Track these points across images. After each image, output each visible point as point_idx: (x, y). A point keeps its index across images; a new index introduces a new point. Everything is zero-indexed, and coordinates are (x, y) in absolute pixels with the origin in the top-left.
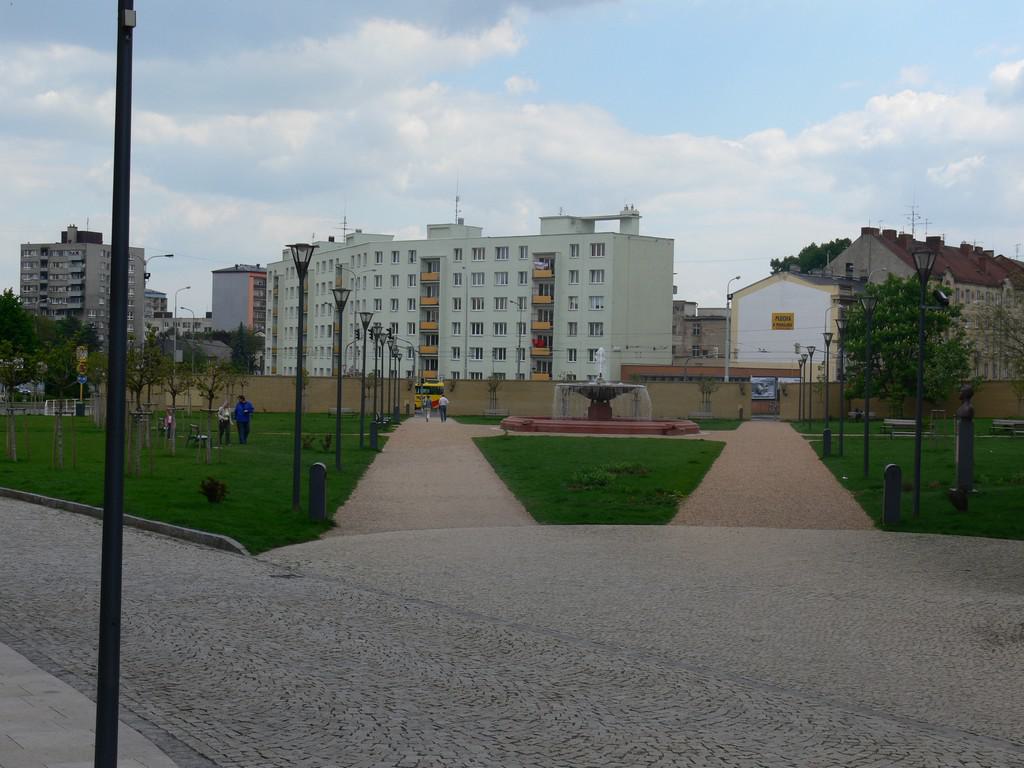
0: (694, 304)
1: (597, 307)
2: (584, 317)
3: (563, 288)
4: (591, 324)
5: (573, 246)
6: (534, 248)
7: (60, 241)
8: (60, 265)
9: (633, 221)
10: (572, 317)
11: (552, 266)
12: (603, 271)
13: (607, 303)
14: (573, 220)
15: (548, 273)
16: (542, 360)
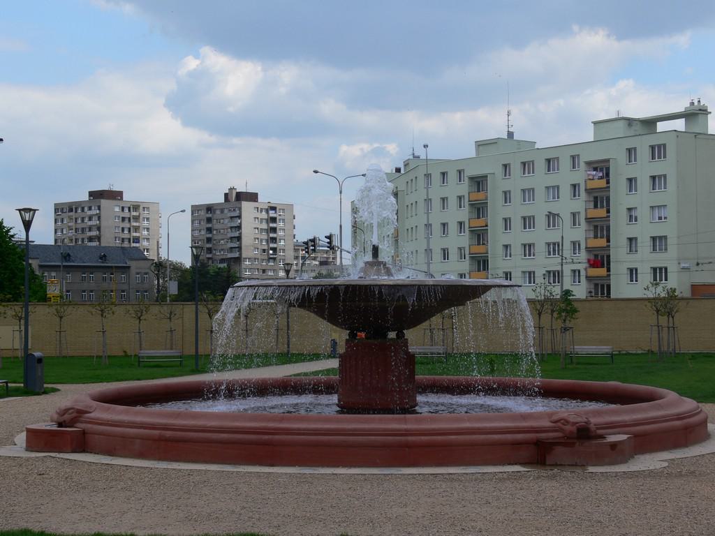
1: (660, 218)
2: (644, 230)
3: (621, 199)
4: (654, 239)
5: (629, 150)
6: (586, 156)
7: (223, 201)
8: (222, 221)
10: (632, 231)
11: (608, 175)
12: (665, 176)
13: (671, 213)
14: (630, 122)
15: (603, 183)
16: (600, 282)
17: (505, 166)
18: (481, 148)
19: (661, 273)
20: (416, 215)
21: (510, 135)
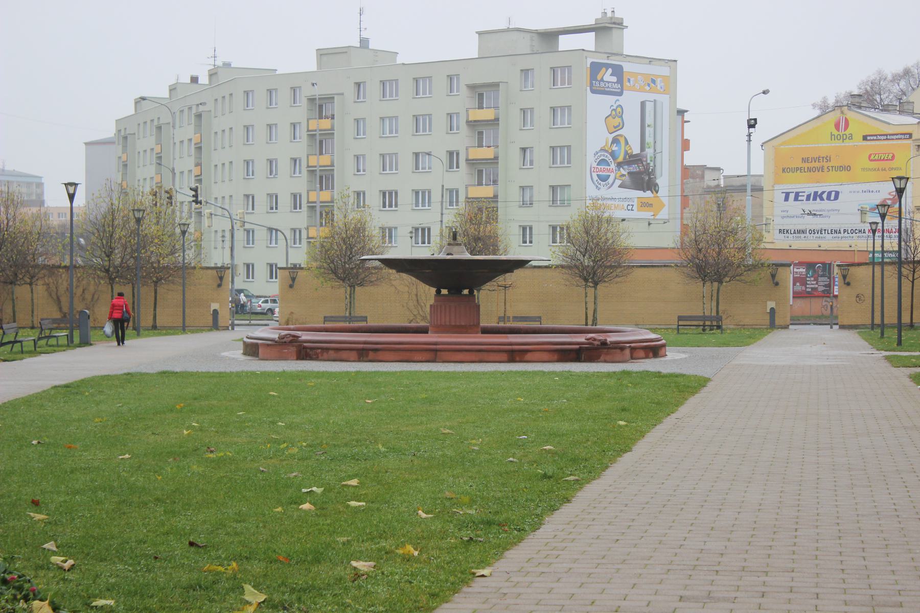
0: (718, 169)
9: (615, 32)
17: (358, 85)
18: (325, 58)
19: (563, 73)
20: (231, 146)
21: (364, 43)
